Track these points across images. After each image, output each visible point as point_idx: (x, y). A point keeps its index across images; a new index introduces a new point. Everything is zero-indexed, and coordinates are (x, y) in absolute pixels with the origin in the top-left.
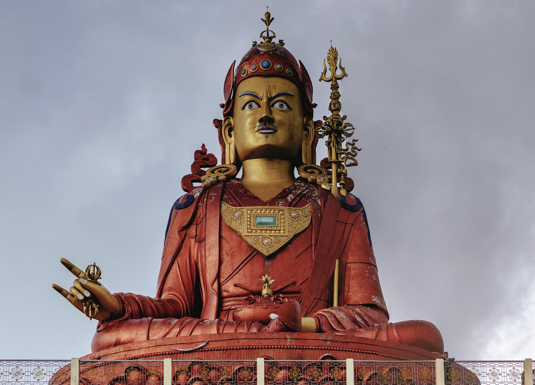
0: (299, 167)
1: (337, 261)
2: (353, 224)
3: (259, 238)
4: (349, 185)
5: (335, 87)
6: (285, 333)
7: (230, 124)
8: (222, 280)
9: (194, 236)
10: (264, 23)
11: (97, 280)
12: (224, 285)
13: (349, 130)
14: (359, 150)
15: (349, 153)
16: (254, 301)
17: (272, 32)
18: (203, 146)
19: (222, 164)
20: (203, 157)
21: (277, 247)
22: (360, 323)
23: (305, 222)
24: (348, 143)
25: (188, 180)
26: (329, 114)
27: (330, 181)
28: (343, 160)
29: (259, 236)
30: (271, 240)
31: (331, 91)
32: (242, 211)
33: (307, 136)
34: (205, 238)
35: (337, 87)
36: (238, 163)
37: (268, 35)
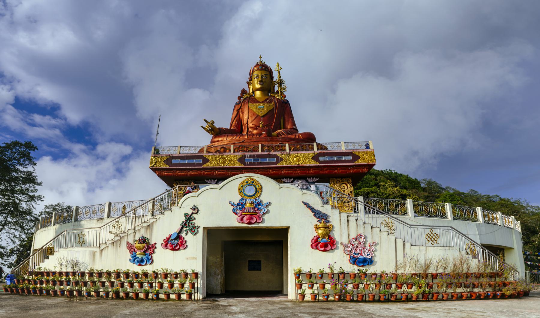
8: (248, 123)
18: (244, 88)
24: (284, 86)
27: (279, 96)
36: (253, 92)
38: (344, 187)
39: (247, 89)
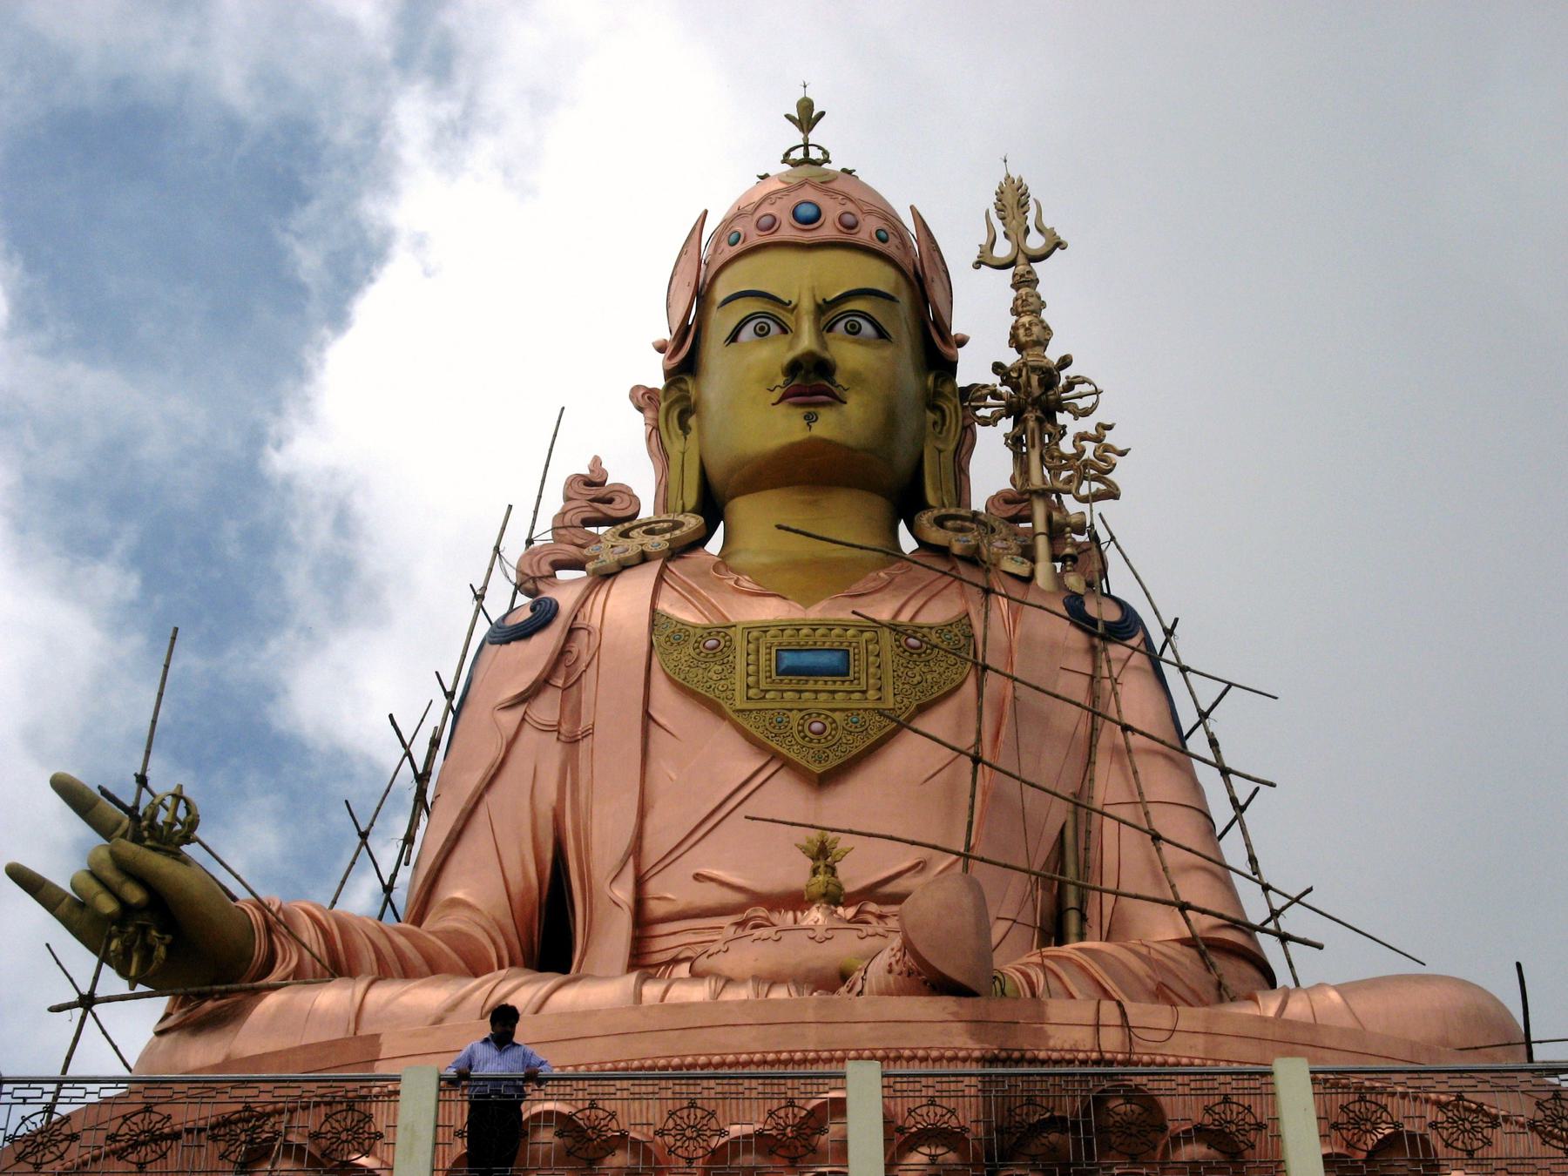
0: (919, 514)
3: (788, 717)
5: (1025, 282)
7: (685, 397)
9: (555, 723)
11: (182, 848)
12: (656, 877)
14: (1123, 454)
15: (1087, 464)
17: (820, 148)
18: (597, 461)
23: (952, 668)
24: (1082, 437)
26: (1010, 357)
27: (1028, 553)
28: (1066, 487)
29: (791, 710)
30: (834, 721)
31: (1013, 293)
32: (726, 635)
33: (940, 427)
34: (593, 726)
35: (1032, 281)
37: (807, 154)
38: (726, 686)
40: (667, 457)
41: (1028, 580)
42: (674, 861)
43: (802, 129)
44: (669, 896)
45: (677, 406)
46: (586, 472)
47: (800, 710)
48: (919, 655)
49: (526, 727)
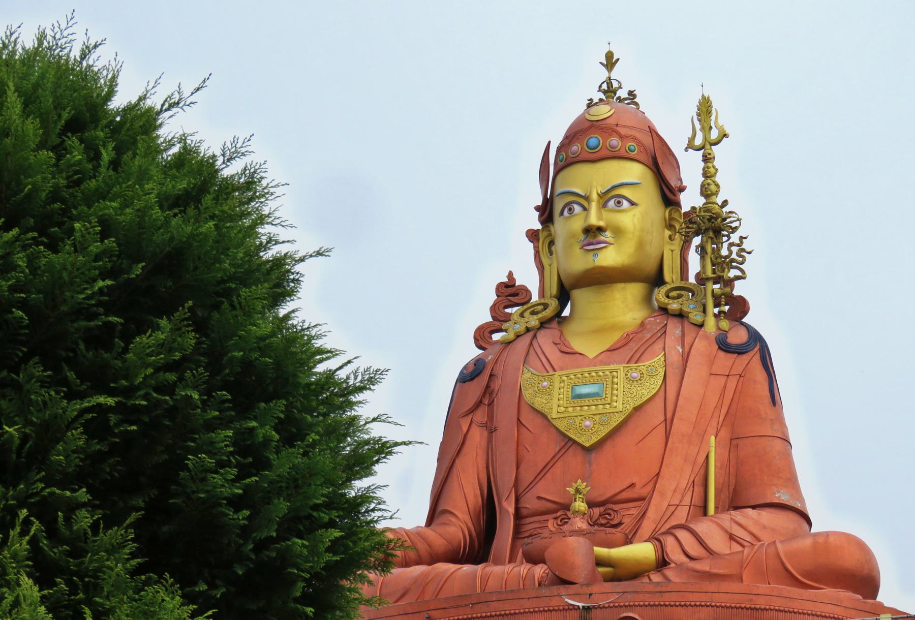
1: (713, 438)
2: (740, 375)
4: (739, 307)
5: (707, 159)
6: (558, 586)
10: (603, 69)
13: (731, 222)
14: (749, 253)
16: (566, 520)
17: (617, 80)
19: (540, 297)
20: (510, 291)
21: (604, 431)
22: (738, 538)
25: (483, 332)
29: (576, 416)
39: (528, 278)
40: (543, 267)
41: (701, 326)
42: (548, 470)
43: (607, 69)
44: (528, 506)
45: (548, 239)
46: (506, 280)
47: (580, 416)
48: (637, 381)
49: (473, 425)
